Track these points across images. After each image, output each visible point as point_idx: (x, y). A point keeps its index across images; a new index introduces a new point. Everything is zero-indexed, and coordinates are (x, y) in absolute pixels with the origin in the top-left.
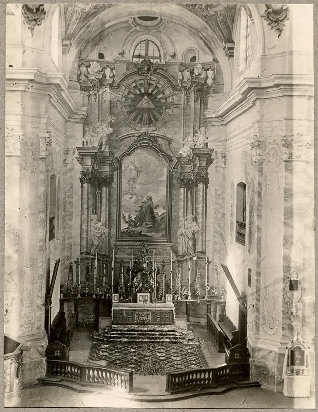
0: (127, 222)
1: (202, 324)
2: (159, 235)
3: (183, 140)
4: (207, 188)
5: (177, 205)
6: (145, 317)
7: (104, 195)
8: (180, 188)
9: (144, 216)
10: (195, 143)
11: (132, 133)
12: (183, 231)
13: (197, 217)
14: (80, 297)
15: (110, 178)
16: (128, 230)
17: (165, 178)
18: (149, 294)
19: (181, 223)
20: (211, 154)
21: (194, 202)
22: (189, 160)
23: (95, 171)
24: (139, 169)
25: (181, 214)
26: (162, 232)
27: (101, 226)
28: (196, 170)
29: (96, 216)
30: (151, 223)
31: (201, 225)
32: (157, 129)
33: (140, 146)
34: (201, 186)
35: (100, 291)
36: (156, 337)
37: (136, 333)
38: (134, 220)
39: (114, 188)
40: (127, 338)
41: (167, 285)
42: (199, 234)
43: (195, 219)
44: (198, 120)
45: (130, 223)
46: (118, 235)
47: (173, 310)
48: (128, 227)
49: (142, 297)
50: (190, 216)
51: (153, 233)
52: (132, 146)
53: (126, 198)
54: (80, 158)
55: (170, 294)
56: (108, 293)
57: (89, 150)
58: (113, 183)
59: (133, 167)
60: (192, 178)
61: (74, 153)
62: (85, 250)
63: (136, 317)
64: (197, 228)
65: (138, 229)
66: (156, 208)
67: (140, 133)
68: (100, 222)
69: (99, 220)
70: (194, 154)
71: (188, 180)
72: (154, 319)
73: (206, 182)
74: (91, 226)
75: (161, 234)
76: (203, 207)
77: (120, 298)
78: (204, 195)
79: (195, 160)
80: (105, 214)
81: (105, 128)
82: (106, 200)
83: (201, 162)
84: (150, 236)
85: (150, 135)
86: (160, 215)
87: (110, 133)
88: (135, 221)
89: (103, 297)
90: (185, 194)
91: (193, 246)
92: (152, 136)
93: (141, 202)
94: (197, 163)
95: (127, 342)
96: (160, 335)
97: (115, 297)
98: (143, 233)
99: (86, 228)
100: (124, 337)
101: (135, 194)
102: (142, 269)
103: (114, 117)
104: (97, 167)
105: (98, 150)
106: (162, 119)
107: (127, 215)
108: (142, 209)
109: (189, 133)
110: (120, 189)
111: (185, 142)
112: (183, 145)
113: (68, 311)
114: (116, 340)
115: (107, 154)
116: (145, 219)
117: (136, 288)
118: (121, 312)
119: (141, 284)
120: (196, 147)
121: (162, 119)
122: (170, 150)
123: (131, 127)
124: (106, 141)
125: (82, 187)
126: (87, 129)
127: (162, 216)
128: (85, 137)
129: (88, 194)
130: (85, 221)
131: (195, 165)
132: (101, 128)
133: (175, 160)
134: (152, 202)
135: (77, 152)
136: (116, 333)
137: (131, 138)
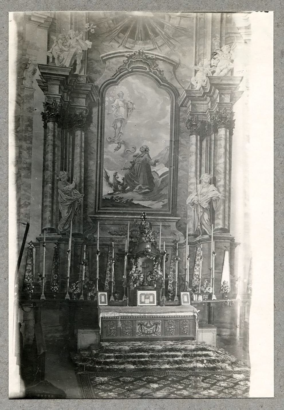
0: (111, 185)
1: (225, 337)
2: (157, 205)
3: (196, 65)
4: (231, 134)
5: (186, 160)
6: (152, 328)
7: (78, 141)
8: (190, 135)
9: (137, 176)
10: (213, 69)
11: (121, 51)
12: (196, 198)
13: (217, 177)
14: (44, 298)
15: (87, 117)
16: (113, 197)
17: (167, 119)
18: (155, 292)
19: (192, 187)
20: (239, 84)
21: (211, 155)
22: (205, 93)
23: (65, 104)
24: (130, 106)
25: (192, 174)
26: (163, 201)
27: (73, 189)
28: (215, 108)
29: (66, 173)
30: (147, 187)
31: (222, 189)
32: (156, 48)
33: (132, 71)
34: (222, 132)
35: (77, 288)
36: (180, 360)
37: (179, 353)
38: (122, 181)
39: (92, 132)
40: (134, 363)
41: (182, 279)
42: (220, 202)
43: (214, 181)
44: (218, 35)
45: (115, 186)
46: (99, 204)
47: (195, 316)
48: (113, 192)
49: (145, 297)
50: (206, 177)
51: (150, 202)
52: (120, 70)
53: (110, 148)
54: (43, 82)
55: (187, 291)
56: (90, 291)
57: (57, 71)
58: (91, 125)
59: (121, 103)
60: (209, 121)
61: (34, 73)
62: (48, 226)
63: (137, 328)
64: (217, 194)
65: (128, 195)
66: (155, 165)
67: (132, 52)
68: (72, 183)
69: (70, 180)
70: (212, 85)
71: (203, 123)
72: (165, 331)
73: (230, 126)
74: (58, 188)
75: (161, 203)
76: (225, 163)
77: (109, 299)
78: (228, 145)
79: (214, 93)
80: (79, 171)
81: (80, 41)
82: (81, 150)
83: (223, 96)
84: (146, 207)
85: (145, 56)
86: (160, 175)
87: (88, 49)
88: (123, 184)
89: (82, 298)
90: (199, 145)
91: (210, 221)
92: (149, 58)
93: (132, 155)
94: (217, 97)
95: (135, 370)
96: (185, 356)
97: (102, 297)
98: (136, 202)
99: (50, 191)
100: (129, 363)
101: (124, 143)
102: (144, 253)
103: (94, 25)
104: (68, 99)
105: (70, 73)
106: (164, 33)
107: (111, 174)
108: (133, 165)
109: (204, 54)
110: (102, 134)
111: (199, 67)
112: (196, 72)
113: (24, 322)
114: (116, 367)
115: (83, 80)
116: (138, 182)
117: (135, 282)
118: (114, 320)
119: (142, 276)
120: (215, 75)
121: (164, 33)
122: (176, 78)
123: (118, 42)
124: (81, 60)
125: (45, 127)
126: (54, 38)
127: (164, 177)
128: (51, 49)
129: (54, 138)
130: (50, 180)
131: (213, 102)
132: (75, 40)
133: (183, 94)
134: (149, 156)
135: (38, 73)
136: (112, 355)
137: (118, 58)
